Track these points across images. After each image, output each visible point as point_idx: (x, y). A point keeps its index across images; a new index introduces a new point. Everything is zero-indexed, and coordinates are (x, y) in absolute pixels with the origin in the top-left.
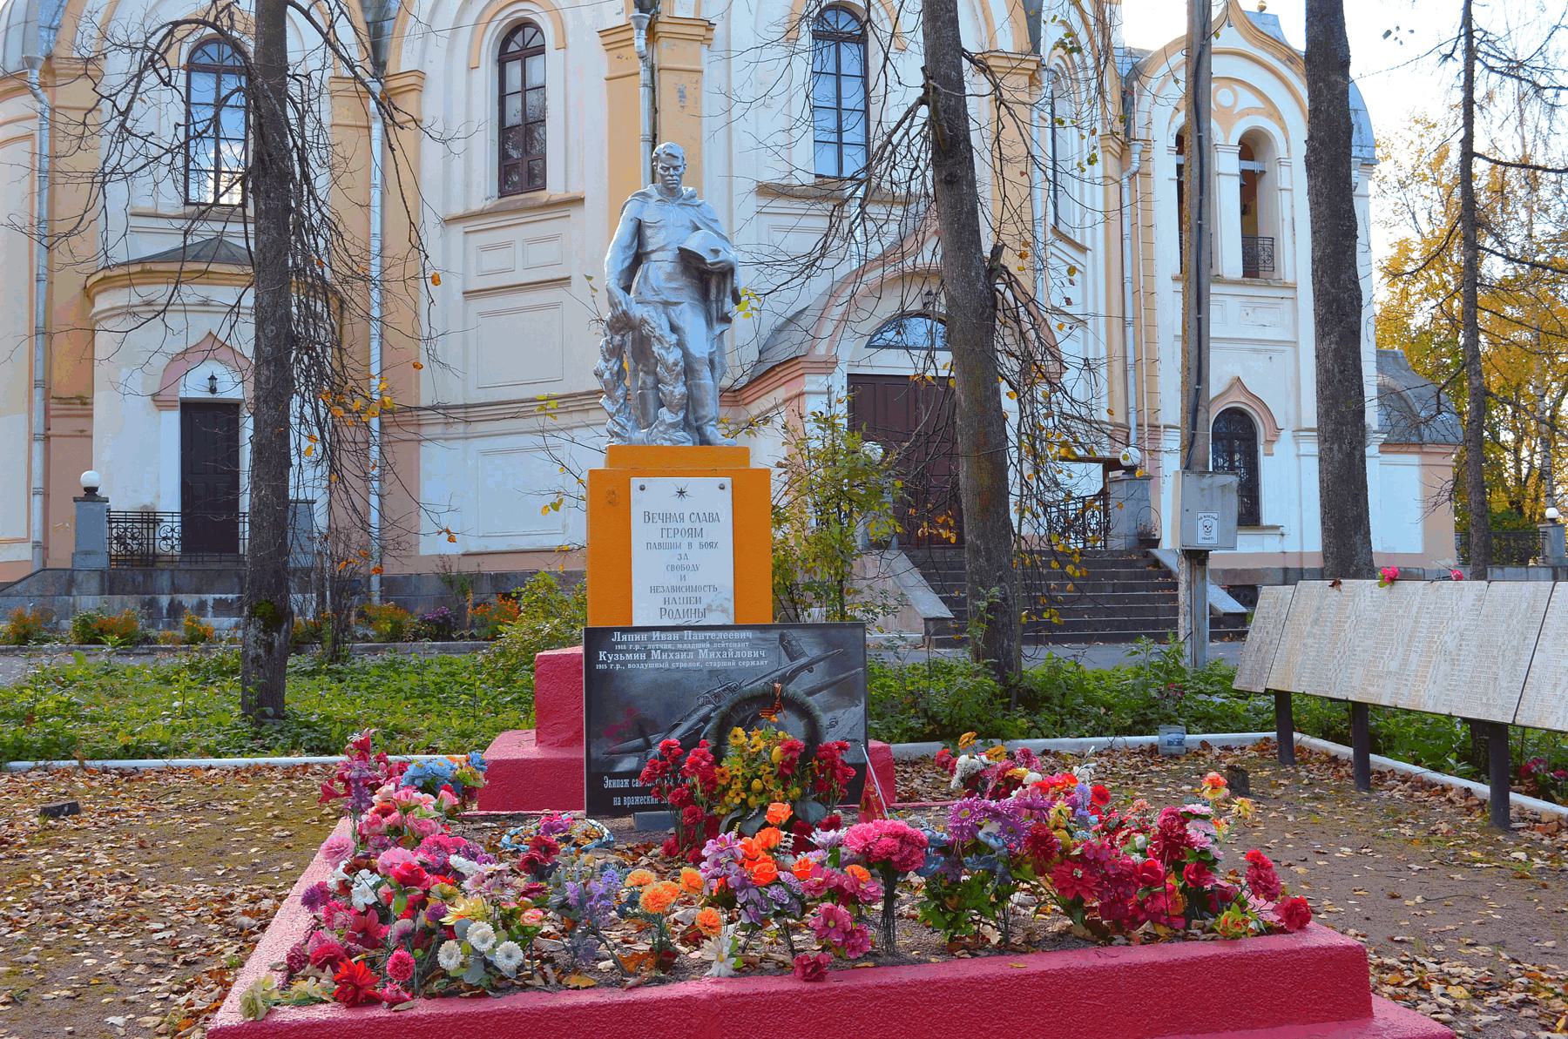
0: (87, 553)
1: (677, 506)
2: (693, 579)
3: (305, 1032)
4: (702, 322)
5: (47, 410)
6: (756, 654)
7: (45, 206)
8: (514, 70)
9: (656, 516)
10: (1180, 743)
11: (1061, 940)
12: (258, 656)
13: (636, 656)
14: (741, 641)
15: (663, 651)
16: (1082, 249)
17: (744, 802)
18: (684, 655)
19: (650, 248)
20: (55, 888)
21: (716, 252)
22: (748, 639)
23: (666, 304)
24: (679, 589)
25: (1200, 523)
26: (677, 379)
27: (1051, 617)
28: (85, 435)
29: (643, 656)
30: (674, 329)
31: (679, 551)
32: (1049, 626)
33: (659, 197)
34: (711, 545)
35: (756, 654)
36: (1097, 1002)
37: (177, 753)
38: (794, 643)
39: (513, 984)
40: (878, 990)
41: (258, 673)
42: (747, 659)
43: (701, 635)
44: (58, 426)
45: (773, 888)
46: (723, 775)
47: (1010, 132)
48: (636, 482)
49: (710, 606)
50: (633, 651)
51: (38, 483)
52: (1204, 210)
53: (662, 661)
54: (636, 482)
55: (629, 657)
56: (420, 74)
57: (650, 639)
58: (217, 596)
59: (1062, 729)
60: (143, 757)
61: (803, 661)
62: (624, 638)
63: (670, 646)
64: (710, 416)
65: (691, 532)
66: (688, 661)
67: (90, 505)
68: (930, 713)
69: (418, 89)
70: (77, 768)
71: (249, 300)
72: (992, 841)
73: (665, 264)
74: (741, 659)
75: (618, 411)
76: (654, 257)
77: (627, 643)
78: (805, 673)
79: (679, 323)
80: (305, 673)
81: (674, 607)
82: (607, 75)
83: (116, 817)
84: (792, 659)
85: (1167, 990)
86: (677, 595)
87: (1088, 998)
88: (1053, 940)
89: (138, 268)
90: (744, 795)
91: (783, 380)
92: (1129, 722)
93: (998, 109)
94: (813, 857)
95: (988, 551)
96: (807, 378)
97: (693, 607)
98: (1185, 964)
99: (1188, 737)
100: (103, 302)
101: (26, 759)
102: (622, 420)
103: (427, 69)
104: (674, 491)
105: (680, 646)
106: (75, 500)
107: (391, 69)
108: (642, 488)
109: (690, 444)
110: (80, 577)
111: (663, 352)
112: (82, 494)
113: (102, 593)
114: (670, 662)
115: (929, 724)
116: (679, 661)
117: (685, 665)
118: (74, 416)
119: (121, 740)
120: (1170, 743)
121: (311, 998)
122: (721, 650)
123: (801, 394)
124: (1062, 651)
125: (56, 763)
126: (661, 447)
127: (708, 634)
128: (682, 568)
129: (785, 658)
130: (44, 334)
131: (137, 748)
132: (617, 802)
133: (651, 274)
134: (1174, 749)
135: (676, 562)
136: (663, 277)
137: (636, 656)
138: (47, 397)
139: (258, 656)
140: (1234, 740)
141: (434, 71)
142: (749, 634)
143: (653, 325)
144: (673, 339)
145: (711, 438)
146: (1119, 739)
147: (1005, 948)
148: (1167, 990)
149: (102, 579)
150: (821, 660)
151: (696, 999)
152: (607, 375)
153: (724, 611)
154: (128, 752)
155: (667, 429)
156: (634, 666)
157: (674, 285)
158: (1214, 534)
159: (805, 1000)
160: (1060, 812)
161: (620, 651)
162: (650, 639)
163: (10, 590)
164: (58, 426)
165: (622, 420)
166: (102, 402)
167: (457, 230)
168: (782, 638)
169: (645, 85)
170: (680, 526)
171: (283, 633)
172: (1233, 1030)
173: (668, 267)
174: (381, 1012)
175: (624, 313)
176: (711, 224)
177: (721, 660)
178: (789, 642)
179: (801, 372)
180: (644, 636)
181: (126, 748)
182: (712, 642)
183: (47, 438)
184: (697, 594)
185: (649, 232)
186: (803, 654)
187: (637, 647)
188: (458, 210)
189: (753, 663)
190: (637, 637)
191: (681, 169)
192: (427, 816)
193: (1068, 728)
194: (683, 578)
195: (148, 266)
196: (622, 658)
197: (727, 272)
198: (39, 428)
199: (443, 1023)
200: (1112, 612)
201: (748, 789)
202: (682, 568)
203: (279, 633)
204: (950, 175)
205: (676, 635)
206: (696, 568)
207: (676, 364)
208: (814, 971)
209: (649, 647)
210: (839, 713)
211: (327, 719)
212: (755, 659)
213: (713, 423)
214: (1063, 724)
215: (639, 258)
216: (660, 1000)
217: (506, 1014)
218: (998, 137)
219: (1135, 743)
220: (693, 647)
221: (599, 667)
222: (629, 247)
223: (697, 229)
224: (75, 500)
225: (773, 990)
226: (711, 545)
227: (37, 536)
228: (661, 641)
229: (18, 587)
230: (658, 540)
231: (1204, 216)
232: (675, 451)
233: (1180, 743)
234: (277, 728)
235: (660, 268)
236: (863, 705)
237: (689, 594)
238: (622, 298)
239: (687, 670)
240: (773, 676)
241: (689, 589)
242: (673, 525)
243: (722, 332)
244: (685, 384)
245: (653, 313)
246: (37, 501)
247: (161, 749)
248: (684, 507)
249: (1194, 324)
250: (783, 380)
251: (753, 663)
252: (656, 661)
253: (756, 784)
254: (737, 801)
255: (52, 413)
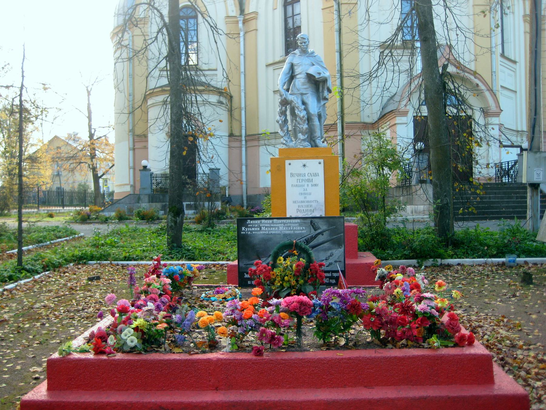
0: (144, 189)
1: (303, 171)
2: (309, 198)
3: (77, 362)
4: (316, 101)
5: (134, 140)
6: (301, 228)
7: (131, 69)
8: (289, 8)
9: (295, 175)
10: (514, 261)
11: (368, 345)
12: (172, 225)
13: (256, 229)
14: (296, 223)
15: (266, 227)
16: (515, 62)
17: (282, 285)
18: (274, 229)
19: (296, 74)
20: (77, 305)
21: (319, 74)
22: (298, 223)
23: (302, 94)
24: (302, 202)
25: (535, 172)
26: (304, 123)
27: (472, 210)
28: (146, 148)
29: (259, 229)
30: (304, 103)
31: (304, 187)
32: (472, 213)
33: (300, 54)
34: (316, 185)
35: (301, 228)
36: (371, 371)
37: (142, 259)
38: (316, 224)
39: (154, 350)
40: (282, 361)
41: (172, 232)
42: (298, 230)
43: (280, 221)
44: (138, 145)
45: (249, 320)
46: (273, 275)
47: (450, 19)
48: (287, 162)
49: (316, 208)
50: (255, 227)
51: (132, 165)
52: (538, 44)
53: (265, 231)
54: (287, 162)
55: (253, 229)
56: (256, 13)
57: (261, 222)
58: (187, 203)
59: (466, 255)
60: (131, 260)
61: (319, 231)
62: (251, 222)
63: (268, 225)
64: (318, 136)
65: (308, 180)
66: (275, 231)
67: (144, 172)
68: (413, 249)
69: (255, 18)
70: (109, 264)
71: (169, 100)
72: (334, 306)
73: (301, 79)
74: (296, 230)
75: (285, 135)
76: (298, 77)
77: (253, 224)
78: (320, 236)
79: (306, 100)
80: (198, 231)
81: (302, 209)
82: (322, 7)
83: (111, 281)
84: (315, 230)
85: (401, 367)
86: (303, 204)
87: (368, 369)
88: (365, 344)
89: (160, 89)
90: (281, 282)
91: (389, 119)
92: (495, 253)
93: (445, 10)
94: (267, 309)
95: (441, 185)
96: (397, 118)
97: (309, 208)
98: (409, 358)
99: (518, 259)
100: (150, 102)
101: (94, 260)
102: (286, 139)
103: (259, 11)
104: (302, 165)
105: (272, 225)
106: (140, 170)
107: (246, 12)
108: (290, 164)
109: (310, 147)
110: (142, 197)
111: (299, 113)
112: (142, 168)
113: (149, 202)
114: (269, 231)
115: (412, 252)
116: (272, 231)
117: (274, 232)
118: (516, 113)
119: (124, 254)
120: (510, 261)
121: (86, 350)
122: (288, 227)
123: (395, 124)
124: (471, 224)
125: (103, 262)
126: (299, 149)
127: (283, 221)
128: (305, 194)
129: (313, 230)
130: (132, 113)
131: (129, 257)
132: (249, 282)
133: (297, 83)
134: (512, 264)
135: (303, 192)
136: (300, 84)
137: (256, 229)
138: (134, 135)
139: (172, 225)
140: (539, 261)
141: (261, 12)
142: (299, 221)
143: (295, 102)
144: (303, 107)
145: (318, 144)
146: (489, 260)
147: (346, 347)
148: (401, 367)
149: (149, 197)
150: (327, 231)
151: (212, 360)
152: (280, 122)
153: (321, 210)
154: (126, 259)
155: (301, 142)
156: (255, 233)
157: (305, 87)
158: (541, 176)
159: (253, 363)
160: (397, 292)
161: (250, 227)
162: (261, 222)
163: (119, 202)
164: (138, 145)
165: (286, 139)
166: (150, 136)
167: (271, 69)
168: (311, 222)
169: (336, 10)
170: (304, 178)
171: (180, 218)
172: (430, 385)
173: (302, 80)
174: (104, 357)
175: (285, 99)
176: (319, 63)
177: (288, 230)
178: (314, 224)
179: (395, 116)
180: (259, 221)
181: (125, 257)
182: (284, 224)
183: (134, 149)
184: (311, 204)
185: (295, 68)
186: (319, 228)
187: (256, 226)
188: (271, 61)
189: (300, 232)
190: (256, 222)
191: (307, 43)
192: (156, 287)
193: (469, 255)
194: (305, 198)
195: (164, 88)
196: (251, 230)
197: (325, 81)
198: (132, 146)
199: (123, 362)
200: (516, 207)
201: (283, 280)
202: (305, 194)
203: (179, 217)
204: (425, 37)
205: (271, 221)
206: (310, 194)
207: (303, 117)
208: (258, 352)
209: (261, 225)
210: (334, 251)
211: (195, 248)
212: (301, 230)
213: (319, 138)
214: (467, 253)
215: (292, 77)
216: (199, 359)
217: (144, 361)
218: (446, 20)
219: (496, 261)
220: (277, 225)
221: (242, 233)
222: (288, 73)
223: (313, 65)
224: (140, 170)
225: (241, 358)
226: (316, 185)
227: (132, 183)
228: (265, 223)
229: (122, 200)
230: (296, 183)
231: (538, 46)
232: (303, 150)
233: (514, 261)
234: (177, 251)
235: (300, 81)
236: (343, 248)
237: (307, 204)
238: (284, 93)
239: (275, 234)
240: (308, 236)
241: (308, 202)
242: (301, 178)
243: (324, 104)
244: (308, 124)
245: (295, 98)
246: (132, 171)
247: (137, 258)
248: (306, 171)
249: (533, 91)
250: (389, 119)
251: (300, 232)
252: (263, 231)
253: (286, 278)
254: (279, 284)
255: (135, 141)
